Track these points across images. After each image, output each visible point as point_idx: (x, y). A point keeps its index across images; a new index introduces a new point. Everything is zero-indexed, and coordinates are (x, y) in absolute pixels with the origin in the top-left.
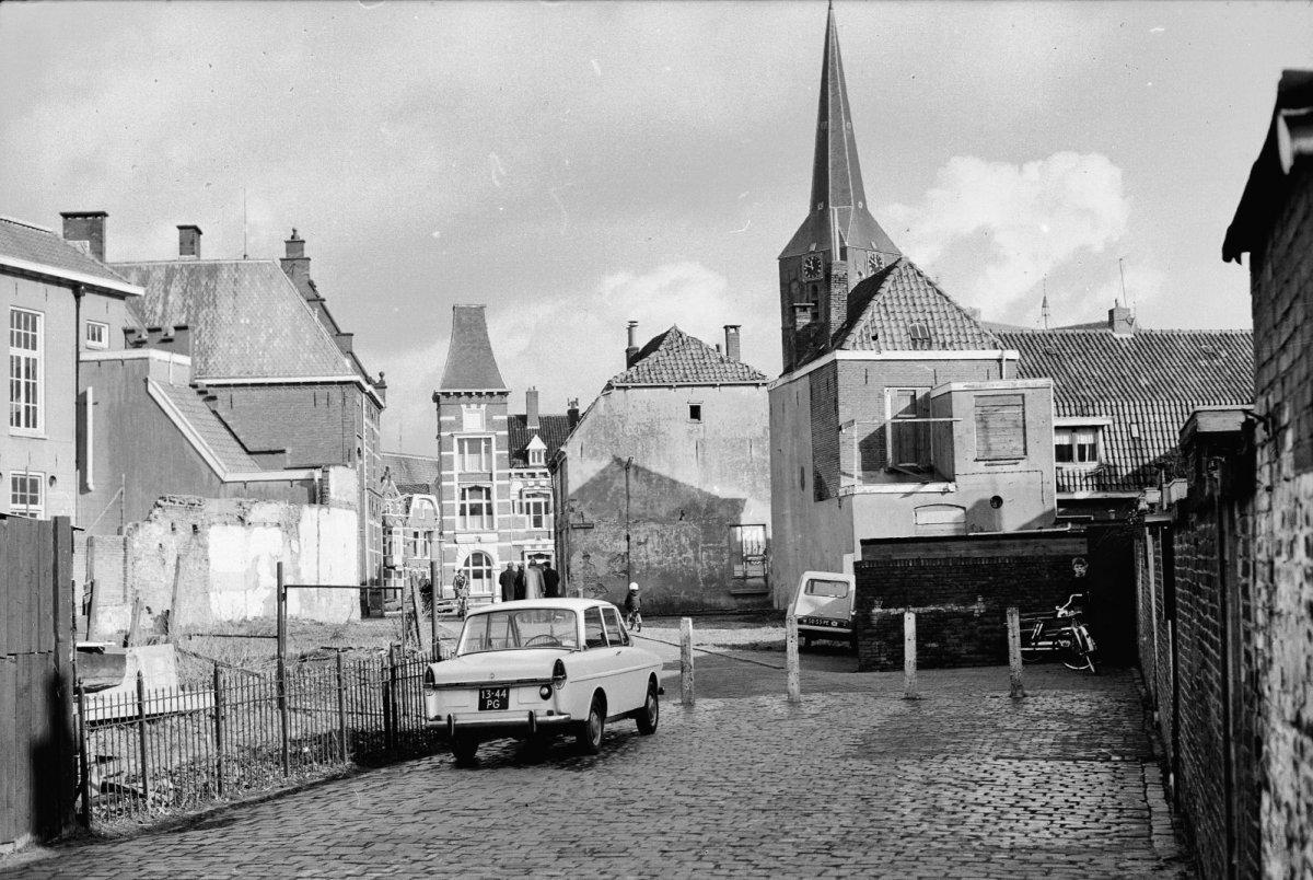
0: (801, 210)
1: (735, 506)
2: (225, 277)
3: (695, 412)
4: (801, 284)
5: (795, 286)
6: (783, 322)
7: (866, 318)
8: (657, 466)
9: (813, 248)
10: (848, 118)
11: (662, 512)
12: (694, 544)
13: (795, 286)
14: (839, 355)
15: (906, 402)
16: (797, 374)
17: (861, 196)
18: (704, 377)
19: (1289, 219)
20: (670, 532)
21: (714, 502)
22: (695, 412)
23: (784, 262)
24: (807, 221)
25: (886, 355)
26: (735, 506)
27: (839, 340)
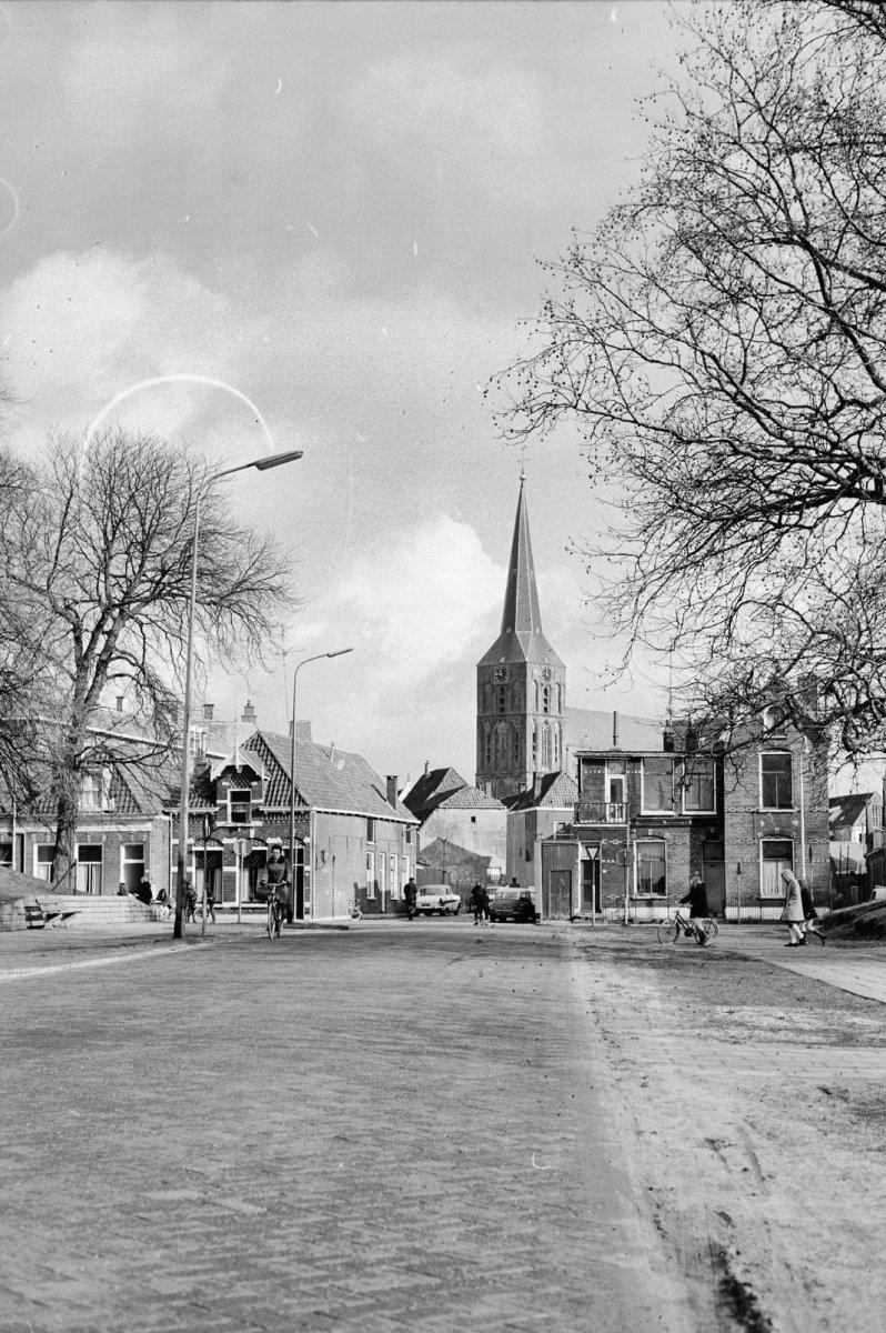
0: (495, 632)
1: (488, 859)
2: (27, 609)
3: (473, 819)
4: (492, 686)
5: (488, 686)
6: (478, 712)
7: (548, 794)
8: (456, 842)
9: (502, 660)
10: (532, 568)
11: (458, 861)
12: (470, 875)
13: (488, 686)
14: (537, 808)
15: (562, 826)
16: (520, 811)
17: (538, 623)
18: (479, 804)
19: (522, 937)
20: (461, 869)
21: (479, 858)
22: (473, 819)
23: (481, 668)
24: (498, 640)
25: (555, 809)
26: (488, 859)
27: (538, 802)
